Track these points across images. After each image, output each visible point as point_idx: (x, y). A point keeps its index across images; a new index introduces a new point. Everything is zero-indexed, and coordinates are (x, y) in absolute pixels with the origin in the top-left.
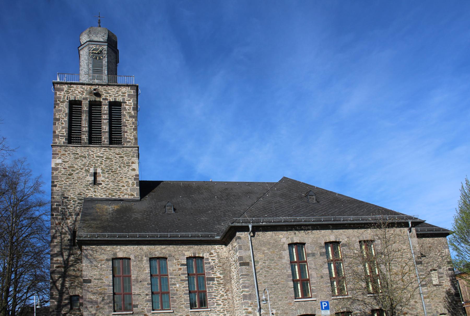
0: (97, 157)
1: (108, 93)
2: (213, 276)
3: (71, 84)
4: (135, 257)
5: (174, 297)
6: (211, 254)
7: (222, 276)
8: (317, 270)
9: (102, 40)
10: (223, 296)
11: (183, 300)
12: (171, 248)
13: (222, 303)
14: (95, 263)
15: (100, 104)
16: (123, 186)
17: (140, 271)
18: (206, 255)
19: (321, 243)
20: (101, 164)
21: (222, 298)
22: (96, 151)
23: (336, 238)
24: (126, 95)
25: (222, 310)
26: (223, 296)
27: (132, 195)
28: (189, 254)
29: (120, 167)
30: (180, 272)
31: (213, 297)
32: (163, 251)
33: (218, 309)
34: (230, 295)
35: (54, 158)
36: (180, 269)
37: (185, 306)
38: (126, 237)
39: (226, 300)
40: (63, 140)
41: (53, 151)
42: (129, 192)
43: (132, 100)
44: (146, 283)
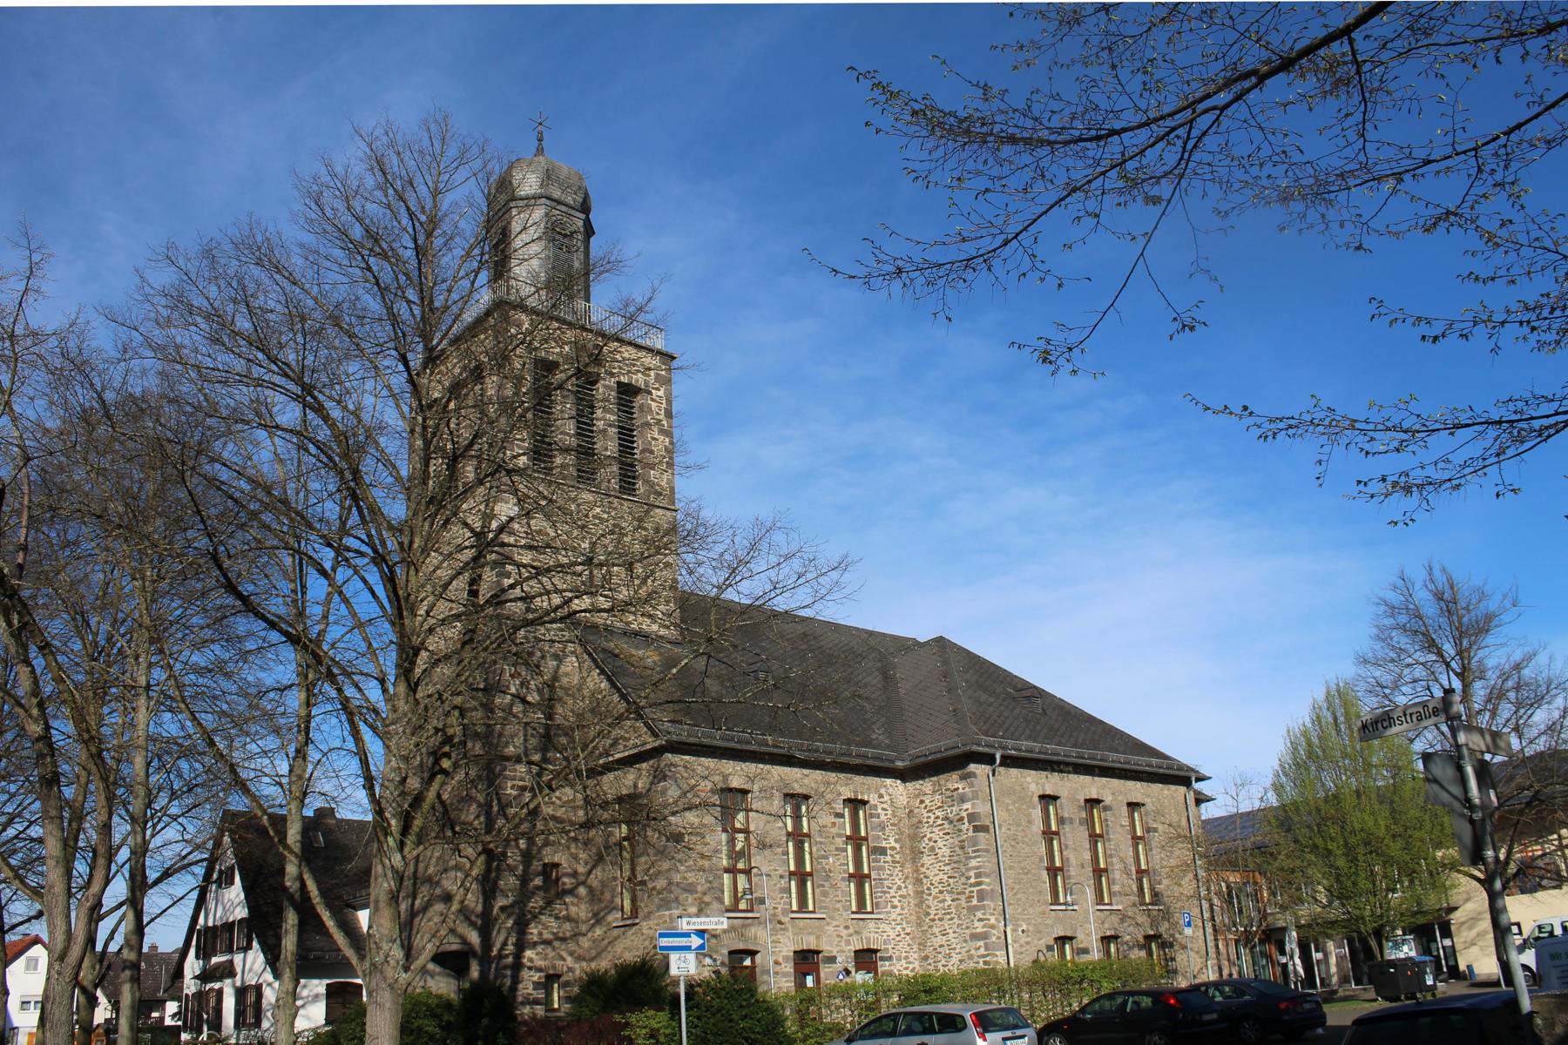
2: (884, 844)
6: (881, 796)
10: (899, 888)
18: (873, 798)
26: (899, 888)
28: (848, 794)
30: (835, 830)
33: (893, 916)
39: (903, 896)
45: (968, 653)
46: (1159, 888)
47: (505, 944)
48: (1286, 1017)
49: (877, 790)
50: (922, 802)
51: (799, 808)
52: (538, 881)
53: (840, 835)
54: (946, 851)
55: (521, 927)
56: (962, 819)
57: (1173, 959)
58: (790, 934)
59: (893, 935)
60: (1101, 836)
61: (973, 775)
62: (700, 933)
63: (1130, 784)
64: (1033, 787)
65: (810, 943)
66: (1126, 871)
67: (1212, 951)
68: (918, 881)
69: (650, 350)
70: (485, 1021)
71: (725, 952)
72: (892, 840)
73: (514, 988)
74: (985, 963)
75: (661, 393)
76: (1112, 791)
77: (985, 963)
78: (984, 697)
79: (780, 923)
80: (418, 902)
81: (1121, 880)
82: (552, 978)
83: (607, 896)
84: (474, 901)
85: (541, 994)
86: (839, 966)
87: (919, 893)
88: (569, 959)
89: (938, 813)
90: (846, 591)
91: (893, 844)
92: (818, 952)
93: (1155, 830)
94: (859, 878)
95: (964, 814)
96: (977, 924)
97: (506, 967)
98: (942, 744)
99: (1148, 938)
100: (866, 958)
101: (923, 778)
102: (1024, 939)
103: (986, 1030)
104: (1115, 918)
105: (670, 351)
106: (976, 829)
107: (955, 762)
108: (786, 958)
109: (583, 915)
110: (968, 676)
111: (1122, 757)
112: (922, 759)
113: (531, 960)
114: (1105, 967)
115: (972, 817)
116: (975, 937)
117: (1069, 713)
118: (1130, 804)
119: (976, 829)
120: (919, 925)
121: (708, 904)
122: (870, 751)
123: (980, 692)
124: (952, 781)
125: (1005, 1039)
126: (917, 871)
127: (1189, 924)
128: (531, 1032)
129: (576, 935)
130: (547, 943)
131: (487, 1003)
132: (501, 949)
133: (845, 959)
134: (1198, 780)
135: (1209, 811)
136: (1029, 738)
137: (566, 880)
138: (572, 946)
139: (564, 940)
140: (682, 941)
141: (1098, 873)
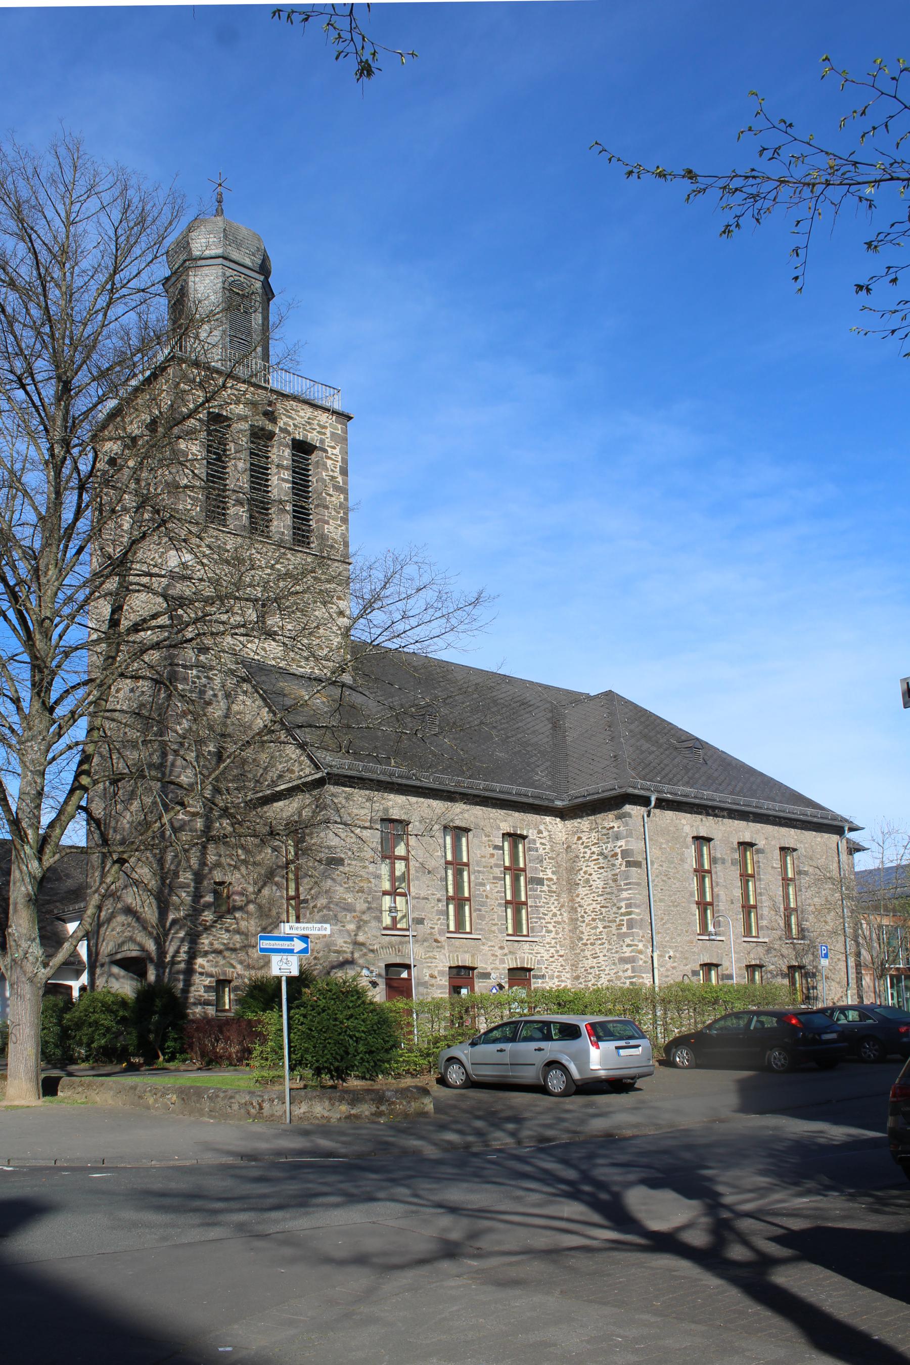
1: (290, 417)
2: (541, 875)
5: (483, 908)
6: (540, 832)
7: (554, 877)
8: (726, 886)
9: (248, 262)
10: (555, 915)
11: (495, 916)
12: (478, 811)
13: (553, 929)
15: (271, 436)
18: (532, 834)
21: (555, 919)
23: (752, 837)
25: (553, 941)
26: (555, 915)
28: (506, 827)
30: (493, 861)
31: (541, 915)
32: (466, 815)
33: (548, 939)
34: (565, 914)
36: (492, 855)
37: (498, 929)
39: (558, 923)
43: (338, 448)
45: (636, 706)
46: (806, 924)
47: (177, 952)
48: (905, 1040)
49: (536, 826)
50: (579, 838)
51: (460, 840)
52: (209, 898)
53: (497, 866)
54: (600, 884)
55: (193, 938)
56: (616, 855)
57: (814, 988)
58: (446, 951)
59: (546, 956)
60: (752, 876)
61: (629, 815)
62: (304, 938)
63: (784, 830)
64: (687, 829)
65: (467, 960)
66: (776, 910)
67: (853, 982)
68: (573, 910)
69: (326, 410)
70: (155, 1018)
71: (383, 965)
72: (549, 872)
73: (186, 991)
74: (631, 983)
75: (337, 451)
76: (767, 837)
77: (631, 983)
78: (646, 746)
79: (436, 941)
80: (103, 914)
81: (769, 916)
82: (222, 983)
83: (274, 913)
84: (150, 914)
85: (212, 996)
86: (493, 981)
87: (573, 920)
88: (239, 967)
89: (594, 849)
90: (476, 625)
91: (550, 876)
92: (473, 969)
93: (806, 873)
94: (517, 905)
95: (618, 851)
96: (625, 949)
97: (178, 972)
98: (601, 786)
99: (791, 968)
100: (520, 975)
101: (581, 817)
102: (670, 964)
103: (600, 1039)
104: (761, 950)
105: (346, 411)
106: (629, 864)
107: (613, 803)
108: (441, 973)
109: (252, 929)
110: (632, 727)
111: (777, 806)
112: (580, 800)
113: (202, 966)
114: (743, 993)
115: (625, 853)
116: (623, 960)
117: (729, 764)
118: (782, 849)
119: (629, 864)
120: (572, 948)
121: (366, 922)
122: (530, 791)
123: (642, 741)
124: (608, 820)
125: (618, 1048)
126: (572, 900)
127: (826, 956)
128: (198, 1029)
129: (245, 947)
130: (219, 952)
131: (158, 1003)
132: (174, 956)
133: (499, 975)
134: (851, 829)
135: (863, 862)
136: (687, 784)
137: (237, 898)
138: (242, 955)
139: (234, 950)
140: (285, 945)
141: (748, 909)
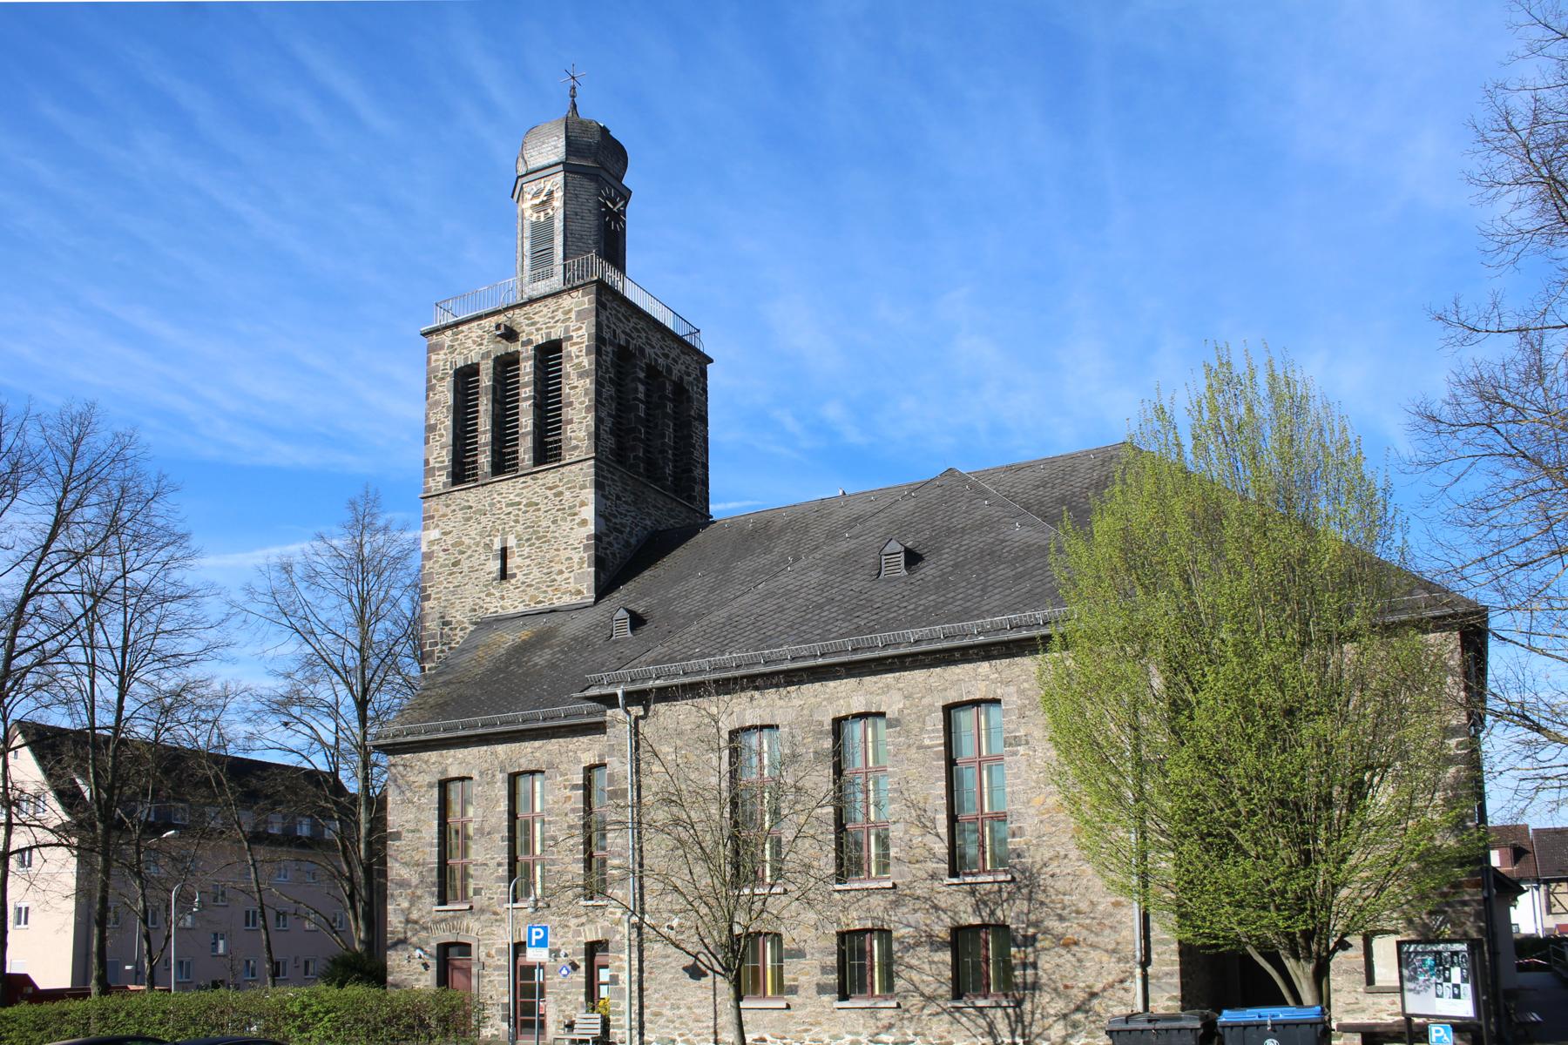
0: (508, 505)
3: (457, 324)
4: (481, 774)
12: (554, 745)
14: (408, 794)
16: (561, 572)
17: (484, 812)
19: (821, 723)
20: (517, 521)
22: (508, 489)
24: (573, 315)
27: (579, 592)
29: (554, 522)
30: (568, 806)
35: (426, 528)
38: (476, 727)
40: (442, 478)
41: (426, 511)
42: (572, 586)
44: (497, 837)
